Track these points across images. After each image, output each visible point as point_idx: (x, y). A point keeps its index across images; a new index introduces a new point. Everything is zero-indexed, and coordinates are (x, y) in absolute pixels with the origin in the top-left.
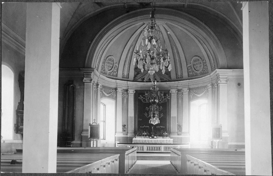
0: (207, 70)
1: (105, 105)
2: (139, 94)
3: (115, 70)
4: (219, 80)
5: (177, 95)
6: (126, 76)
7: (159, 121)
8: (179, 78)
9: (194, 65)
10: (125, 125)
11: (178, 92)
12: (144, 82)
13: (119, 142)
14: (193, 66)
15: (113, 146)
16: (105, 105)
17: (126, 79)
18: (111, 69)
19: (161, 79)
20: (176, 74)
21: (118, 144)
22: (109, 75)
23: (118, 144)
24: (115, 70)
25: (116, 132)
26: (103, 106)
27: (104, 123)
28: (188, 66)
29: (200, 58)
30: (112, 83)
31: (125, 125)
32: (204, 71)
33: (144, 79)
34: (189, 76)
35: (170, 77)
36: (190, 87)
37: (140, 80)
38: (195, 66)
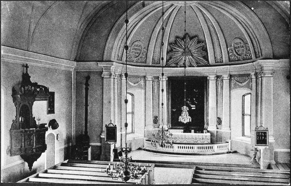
0: (251, 55)
1: (132, 95)
2: (173, 82)
3: (144, 56)
4: (263, 72)
5: (216, 82)
6: (156, 62)
7: (191, 119)
8: (218, 62)
9: (235, 48)
10: (157, 117)
11: (217, 78)
12: (178, 67)
13: (147, 139)
14: (235, 49)
15: (183, 75)
16: (132, 95)
17: (156, 64)
18: (139, 56)
19: (197, 63)
20: (215, 58)
21: (146, 140)
22: (137, 62)
23: (146, 140)
24: (144, 56)
25: (145, 125)
26: (131, 96)
27: (133, 114)
28: (228, 49)
29: (242, 40)
30: (141, 71)
31: (157, 117)
32: (247, 56)
33: (177, 64)
34: (230, 60)
35: (207, 60)
36: (231, 74)
37: (174, 65)
38: (236, 50)
